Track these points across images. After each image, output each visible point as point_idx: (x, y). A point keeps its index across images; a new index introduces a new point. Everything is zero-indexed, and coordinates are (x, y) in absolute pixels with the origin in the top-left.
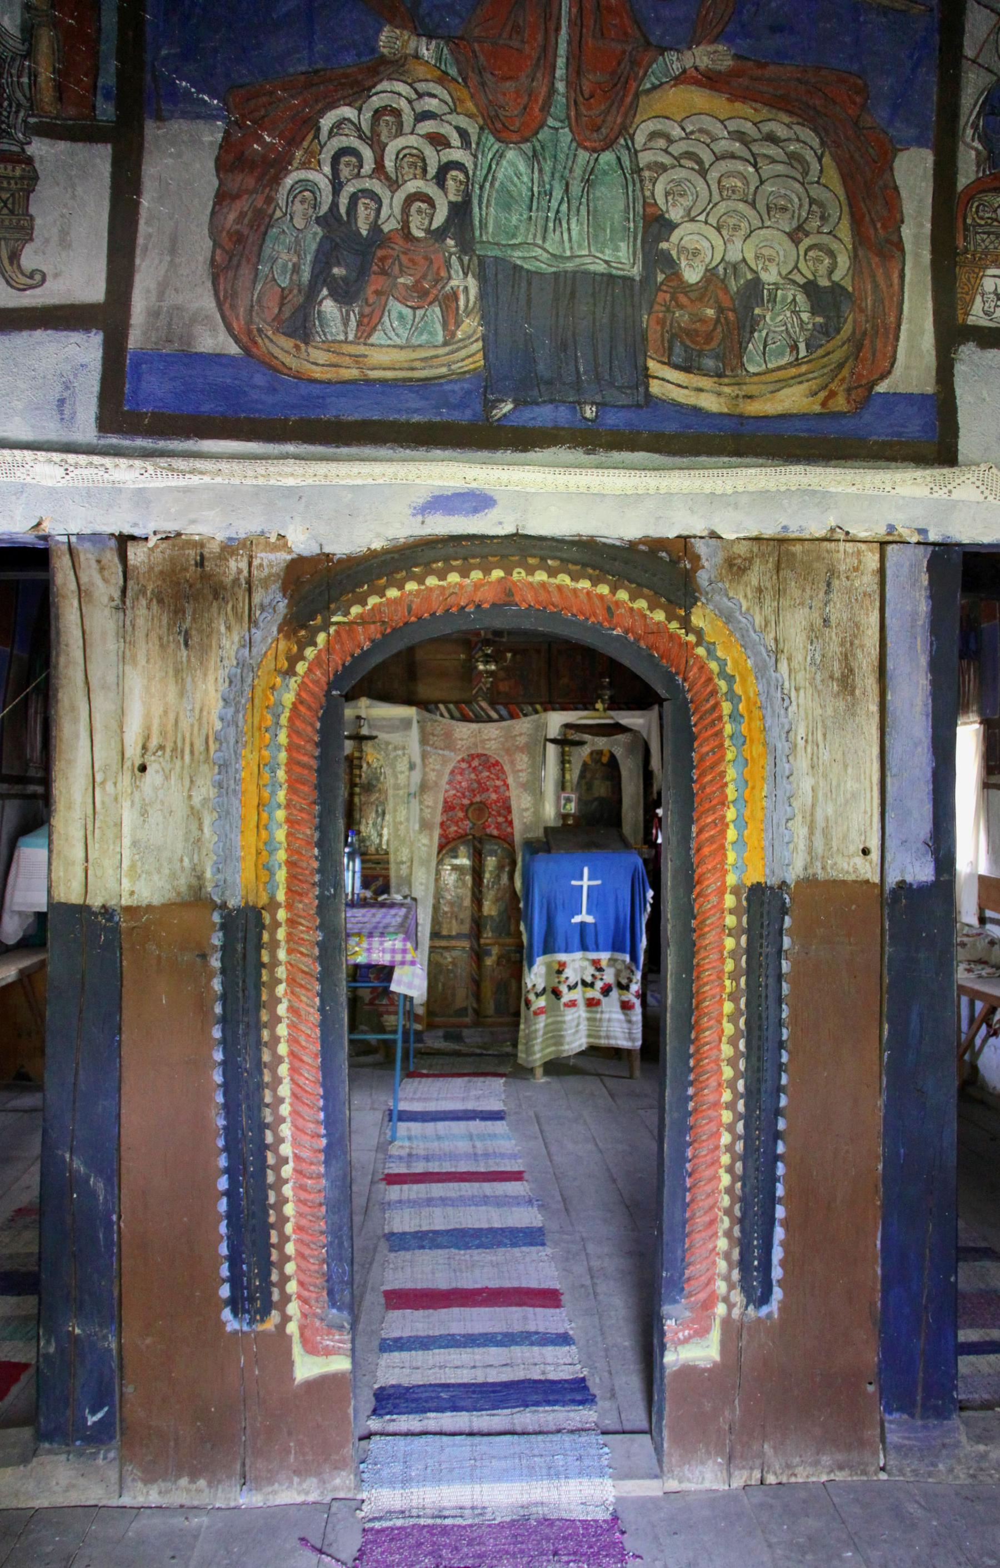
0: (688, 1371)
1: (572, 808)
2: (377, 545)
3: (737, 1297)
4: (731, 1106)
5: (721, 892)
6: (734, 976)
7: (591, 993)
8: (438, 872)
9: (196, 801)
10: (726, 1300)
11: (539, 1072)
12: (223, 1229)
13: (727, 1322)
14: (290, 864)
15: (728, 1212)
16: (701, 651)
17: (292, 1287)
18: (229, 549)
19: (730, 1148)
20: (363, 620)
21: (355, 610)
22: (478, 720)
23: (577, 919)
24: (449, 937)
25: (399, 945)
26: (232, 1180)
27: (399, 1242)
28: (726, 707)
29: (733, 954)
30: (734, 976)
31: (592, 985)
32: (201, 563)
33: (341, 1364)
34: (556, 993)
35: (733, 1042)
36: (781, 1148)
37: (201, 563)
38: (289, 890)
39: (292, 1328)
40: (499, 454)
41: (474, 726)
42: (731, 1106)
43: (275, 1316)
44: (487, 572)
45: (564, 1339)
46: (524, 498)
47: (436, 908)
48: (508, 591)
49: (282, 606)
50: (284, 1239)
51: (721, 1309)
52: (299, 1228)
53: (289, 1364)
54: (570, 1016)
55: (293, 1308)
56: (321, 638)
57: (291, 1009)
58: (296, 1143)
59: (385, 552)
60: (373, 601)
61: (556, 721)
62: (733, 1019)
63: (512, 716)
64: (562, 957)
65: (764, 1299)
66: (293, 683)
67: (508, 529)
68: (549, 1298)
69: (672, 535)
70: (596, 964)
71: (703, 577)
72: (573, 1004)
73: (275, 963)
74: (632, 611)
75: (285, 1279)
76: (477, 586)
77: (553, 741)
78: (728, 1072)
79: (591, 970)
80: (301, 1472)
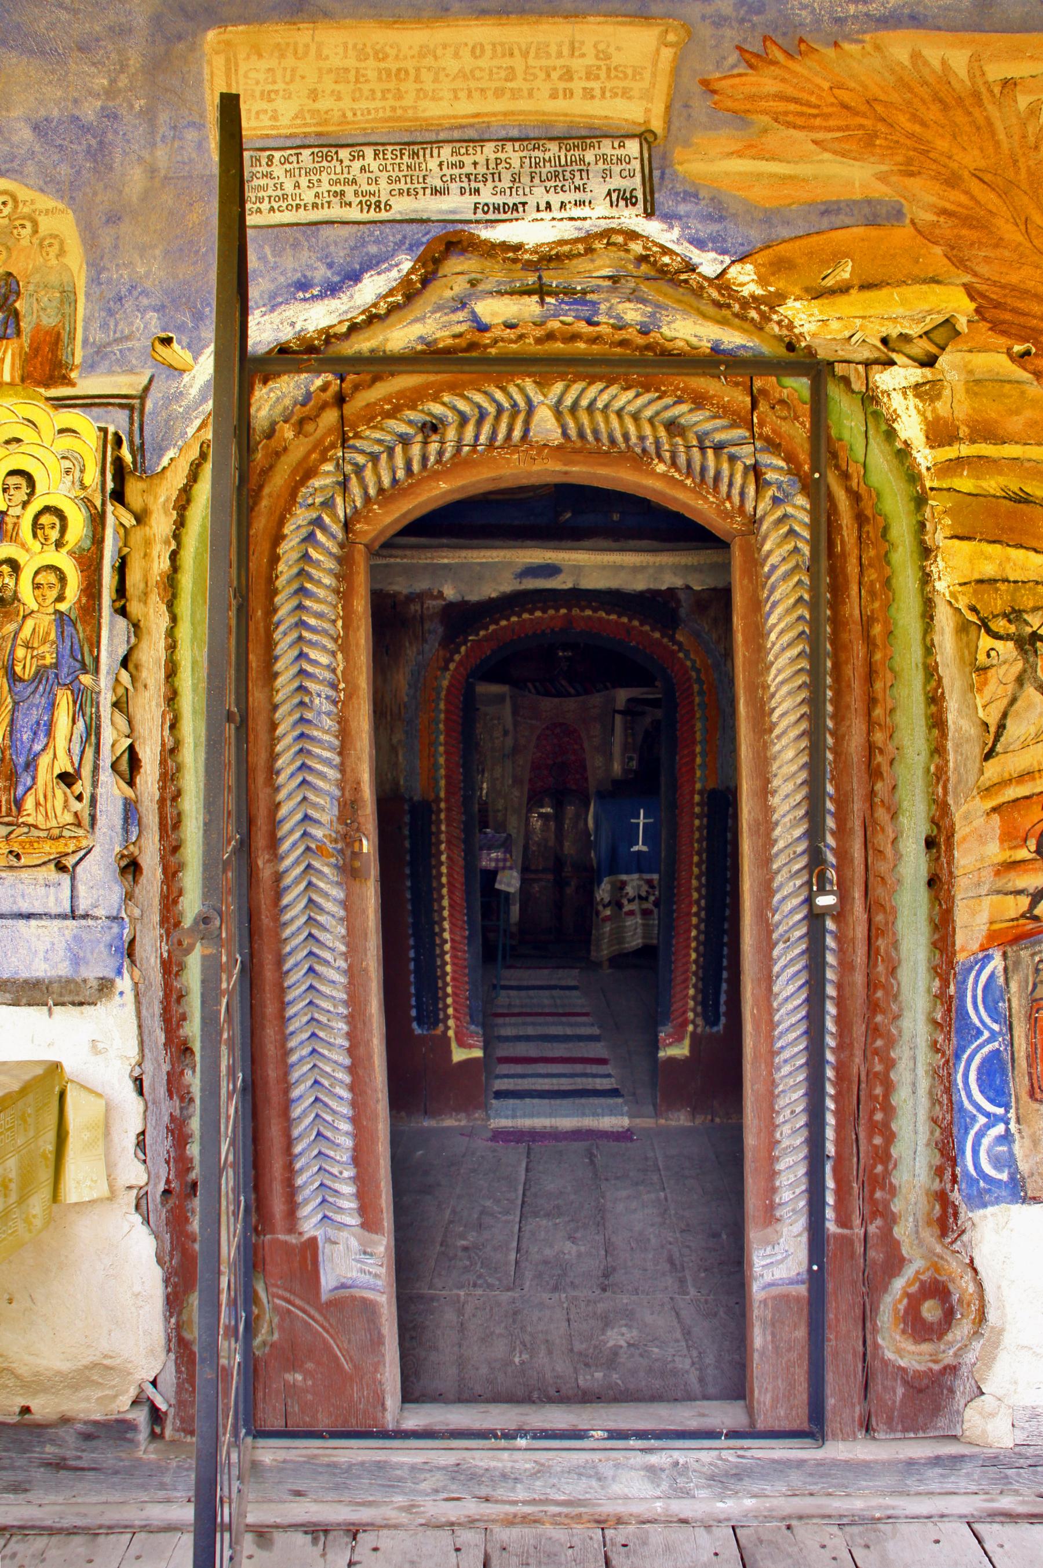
0: (671, 1060)
1: (634, 764)
2: (494, 595)
3: (700, 1021)
4: (697, 914)
5: (692, 792)
6: (699, 841)
7: (646, 905)
8: (527, 820)
9: (395, 741)
10: (693, 1022)
11: (606, 964)
12: (412, 978)
13: (693, 1034)
14: (447, 777)
15: (695, 974)
16: (681, 655)
17: (450, 1011)
18: (411, 598)
19: (696, 938)
20: (487, 638)
21: (482, 633)
22: (559, 695)
23: (635, 848)
24: (536, 871)
25: (500, 855)
26: (417, 953)
27: (507, 1039)
28: (696, 687)
29: (699, 829)
30: (699, 841)
31: (646, 899)
32: (394, 606)
33: (478, 1053)
34: (620, 906)
35: (698, 878)
36: (726, 939)
37: (394, 606)
38: (447, 792)
39: (451, 1033)
40: (563, 544)
41: (556, 700)
42: (697, 914)
43: (441, 1027)
44: (557, 610)
45: (609, 1076)
46: (578, 569)
47: (526, 847)
48: (569, 619)
49: (440, 630)
50: (446, 984)
51: (691, 1028)
52: (453, 979)
53: (450, 1052)
54: (629, 922)
55: (451, 1023)
56: (463, 649)
57: (449, 858)
58: (451, 932)
59: (498, 599)
60: (492, 627)
61: (622, 696)
62: (698, 865)
63: (587, 692)
64: (624, 877)
65: (715, 1022)
66: (448, 675)
67: (569, 585)
68: (602, 1061)
69: (664, 587)
70: (649, 882)
71: (683, 612)
72: (631, 913)
73: (440, 832)
74: (645, 631)
75: (446, 1006)
76: (552, 618)
77: (619, 712)
78: (695, 895)
79: (645, 888)
80: (458, 1109)
